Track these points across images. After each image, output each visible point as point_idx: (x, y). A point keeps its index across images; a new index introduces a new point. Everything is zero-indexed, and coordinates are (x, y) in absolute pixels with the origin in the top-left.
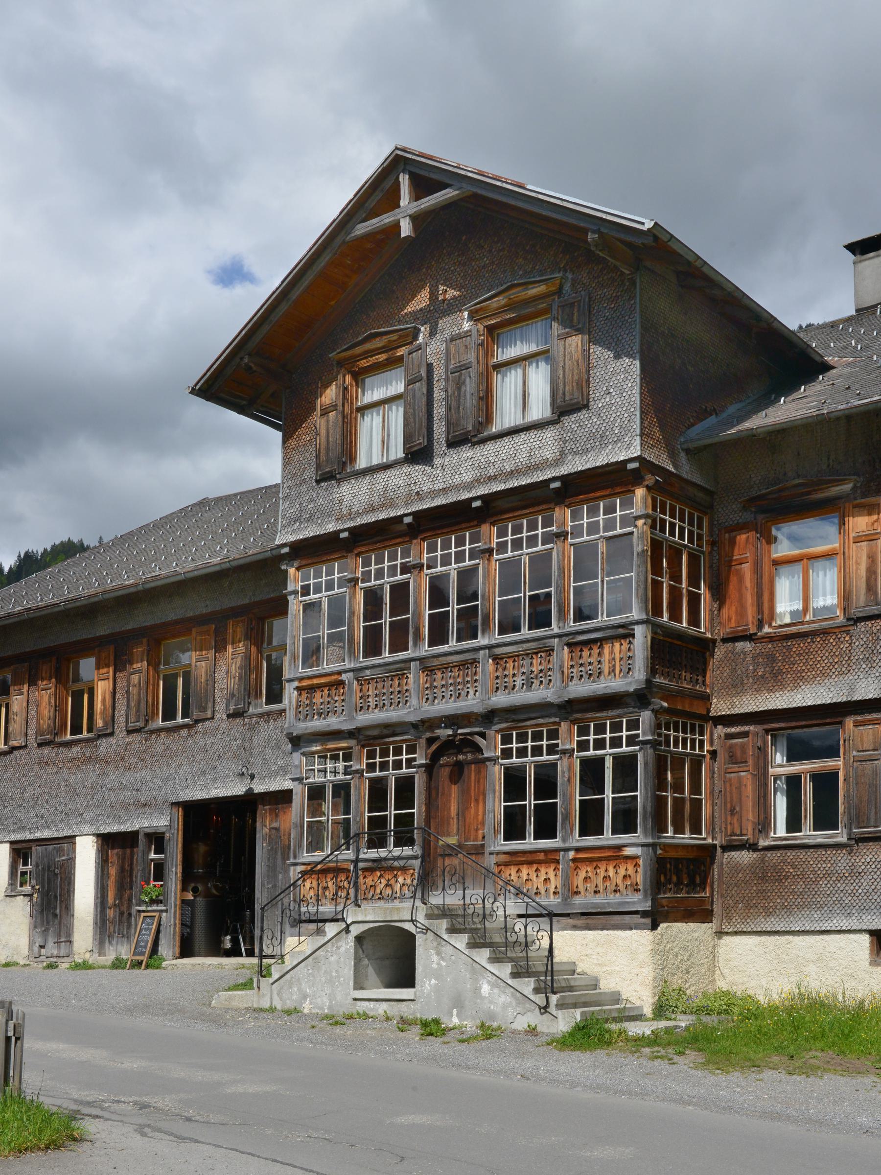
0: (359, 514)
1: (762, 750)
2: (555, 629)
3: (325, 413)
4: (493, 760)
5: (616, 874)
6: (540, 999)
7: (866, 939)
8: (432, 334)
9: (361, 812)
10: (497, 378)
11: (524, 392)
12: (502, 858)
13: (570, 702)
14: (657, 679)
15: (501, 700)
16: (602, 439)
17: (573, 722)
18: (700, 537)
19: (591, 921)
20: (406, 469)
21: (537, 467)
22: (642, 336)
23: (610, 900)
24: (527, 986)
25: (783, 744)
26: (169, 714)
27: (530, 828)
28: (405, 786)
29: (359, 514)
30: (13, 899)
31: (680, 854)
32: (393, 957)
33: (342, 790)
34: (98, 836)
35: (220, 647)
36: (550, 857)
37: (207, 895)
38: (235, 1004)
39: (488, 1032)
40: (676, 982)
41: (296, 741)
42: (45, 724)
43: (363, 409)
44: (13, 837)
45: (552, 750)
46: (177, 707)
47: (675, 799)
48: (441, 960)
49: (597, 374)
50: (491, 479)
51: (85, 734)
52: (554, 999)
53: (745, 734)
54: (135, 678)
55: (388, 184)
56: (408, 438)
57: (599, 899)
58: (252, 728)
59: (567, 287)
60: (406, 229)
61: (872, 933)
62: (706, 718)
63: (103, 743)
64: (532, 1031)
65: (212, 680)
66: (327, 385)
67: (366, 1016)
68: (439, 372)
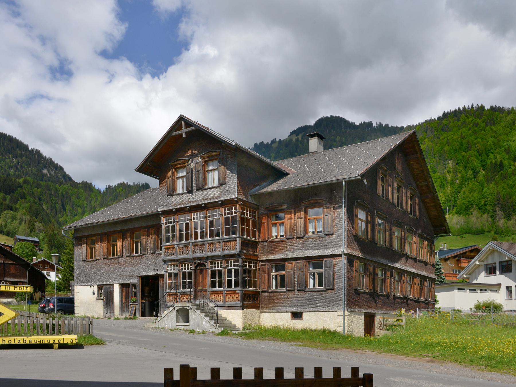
0: (177, 205)
1: (269, 269)
2: (221, 238)
3: (168, 178)
4: (209, 269)
5: (235, 297)
6: (215, 325)
7: (290, 314)
8: (192, 162)
9: (180, 280)
10: (207, 174)
11: (213, 178)
12: (211, 292)
13: (224, 255)
14: (243, 251)
15: (210, 254)
16: (229, 192)
17: (225, 260)
18: (255, 216)
19: (230, 308)
20: (187, 195)
21: (216, 198)
22: (237, 168)
23: (233, 303)
24: (212, 322)
25: (274, 268)
26: (137, 252)
27: (217, 285)
28: (190, 273)
29: (177, 205)
31: (249, 293)
32: (184, 315)
33: (176, 274)
34: (120, 284)
35: (148, 236)
36: (221, 293)
37: (149, 301)
38: (150, 326)
39: (204, 332)
40: (249, 323)
41: (165, 262)
42: (105, 253)
43: (178, 178)
44: (98, 284)
45: (221, 267)
46: (138, 250)
47: (249, 280)
48: (195, 316)
49: (228, 176)
50: (206, 199)
51: (115, 257)
52: (218, 325)
53: (265, 265)
54: (127, 242)
55: (180, 123)
56: (187, 187)
57: (231, 303)
58: (157, 257)
59: (221, 153)
60: (184, 136)
61: (291, 312)
62: (257, 260)
63: (120, 259)
64: (213, 332)
65: (147, 244)
66: (169, 171)
67: (179, 329)
68: (194, 171)
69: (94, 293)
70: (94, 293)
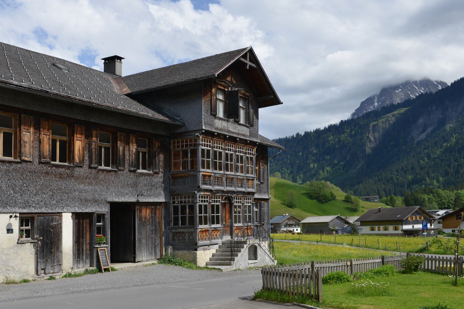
28: (218, 206)
30: (23, 245)
34: (73, 213)
69: (10, 231)
70: (10, 231)
